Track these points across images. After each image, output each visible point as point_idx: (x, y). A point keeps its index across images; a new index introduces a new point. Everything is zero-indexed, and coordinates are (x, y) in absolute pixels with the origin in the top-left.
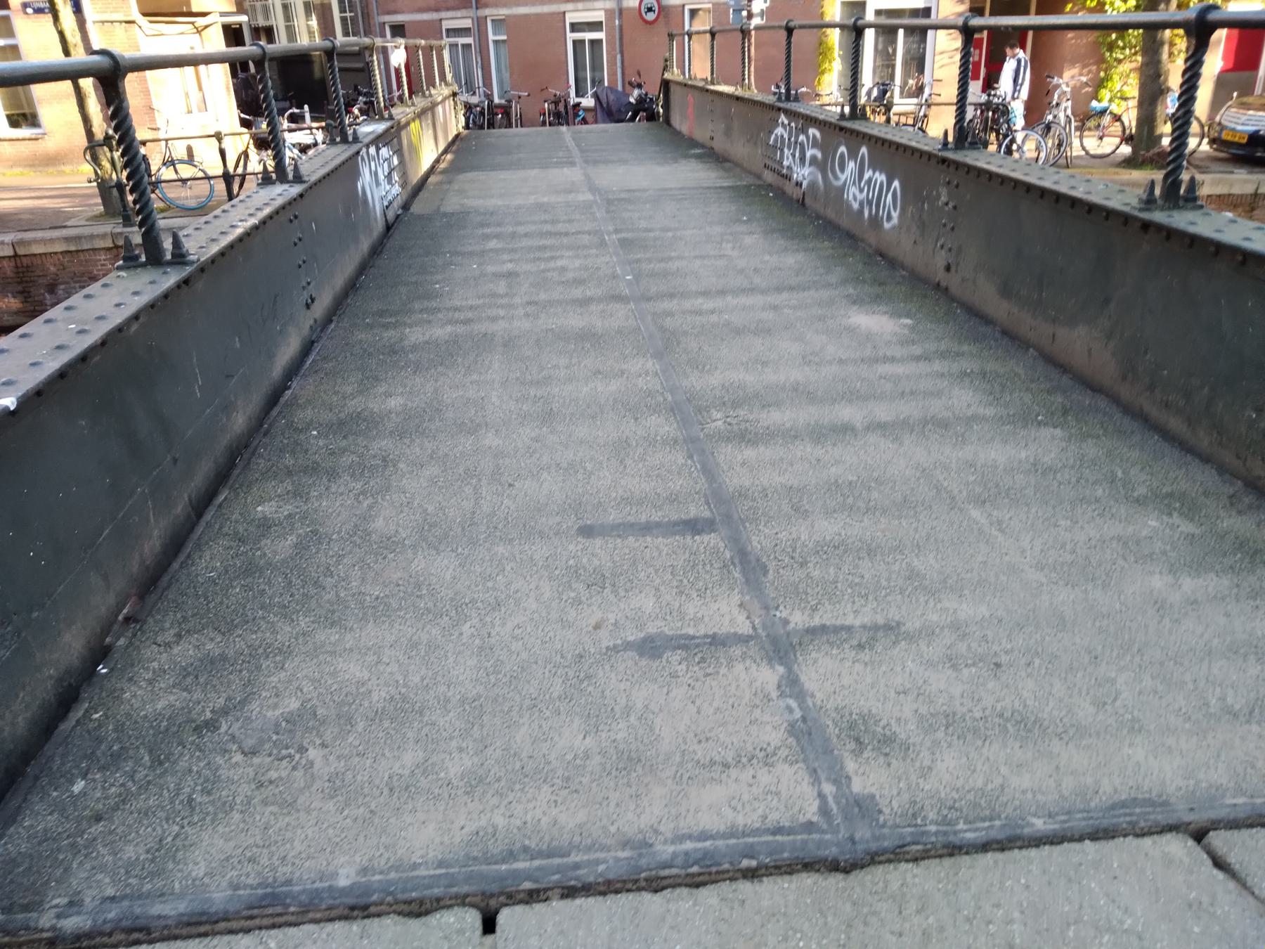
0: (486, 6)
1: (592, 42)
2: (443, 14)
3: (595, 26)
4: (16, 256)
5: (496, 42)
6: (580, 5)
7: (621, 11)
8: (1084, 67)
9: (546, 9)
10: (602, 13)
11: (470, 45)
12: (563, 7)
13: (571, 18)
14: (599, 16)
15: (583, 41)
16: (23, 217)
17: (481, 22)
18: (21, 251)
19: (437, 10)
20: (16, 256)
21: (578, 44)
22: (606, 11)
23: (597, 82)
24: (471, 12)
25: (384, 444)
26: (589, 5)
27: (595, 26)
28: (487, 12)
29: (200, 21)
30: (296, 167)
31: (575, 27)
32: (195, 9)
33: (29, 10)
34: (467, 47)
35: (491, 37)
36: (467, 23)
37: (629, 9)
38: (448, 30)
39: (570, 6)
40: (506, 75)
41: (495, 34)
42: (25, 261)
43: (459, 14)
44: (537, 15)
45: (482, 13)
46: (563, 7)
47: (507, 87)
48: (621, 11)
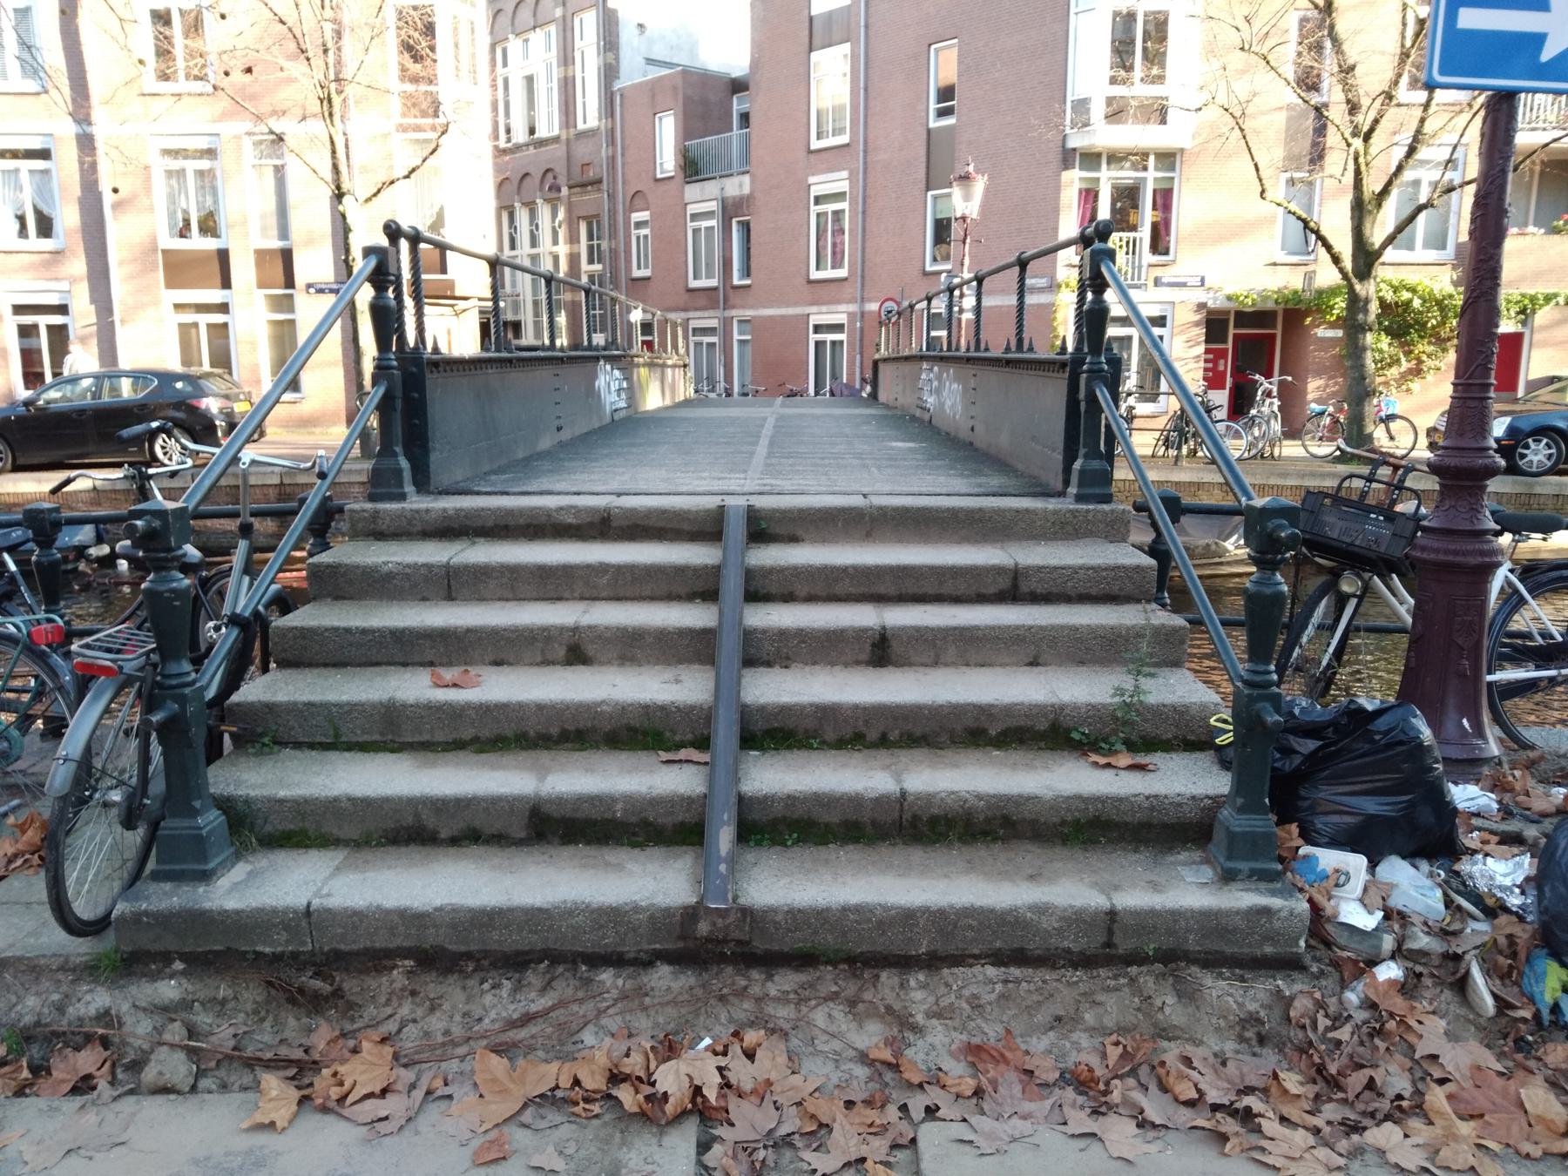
0: (733, 307)
1: (834, 343)
2: (691, 314)
3: (838, 328)
4: (282, 484)
5: (741, 342)
6: (824, 308)
7: (863, 314)
8: (1330, 378)
9: (791, 311)
10: (844, 316)
11: (714, 344)
12: (807, 310)
13: (814, 320)
14: (841, 318)
15: (824, 342)
16: (1007, 660)
17: (727, 323)
18: (286, 481)
19: (685, 310)
20: (282, 484)
21: (819, 345)
22: (849, 314)
23: (835, 376)
24: (718, 313)
25: (1198, 317)
26: (833, 308)
27: (838, 328)
28: (734, 312)
29: (461, 304)
30: (435, 343)
31: (817, 329)
32: (457, 294)
33: (312, 290)
34: (711, 345)
35: (736, 336)
36: (714, 323)
37: (871, 312)
38: (694, 330)
39: (814, 309)
40: (749, 373)
41: (740, 333)
42: (288, 490)
43: (706, 314)
44: (783, 317)
45: (728, 313)
46: (807, 310)
47: (748, 380)
48: (863, 314)
